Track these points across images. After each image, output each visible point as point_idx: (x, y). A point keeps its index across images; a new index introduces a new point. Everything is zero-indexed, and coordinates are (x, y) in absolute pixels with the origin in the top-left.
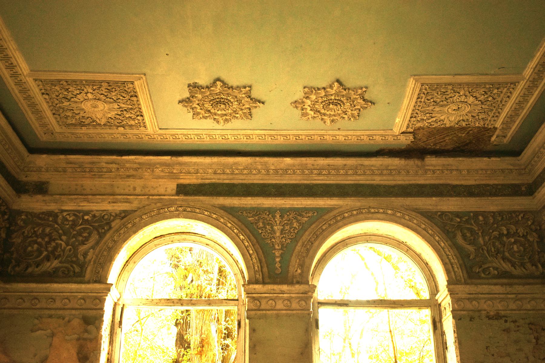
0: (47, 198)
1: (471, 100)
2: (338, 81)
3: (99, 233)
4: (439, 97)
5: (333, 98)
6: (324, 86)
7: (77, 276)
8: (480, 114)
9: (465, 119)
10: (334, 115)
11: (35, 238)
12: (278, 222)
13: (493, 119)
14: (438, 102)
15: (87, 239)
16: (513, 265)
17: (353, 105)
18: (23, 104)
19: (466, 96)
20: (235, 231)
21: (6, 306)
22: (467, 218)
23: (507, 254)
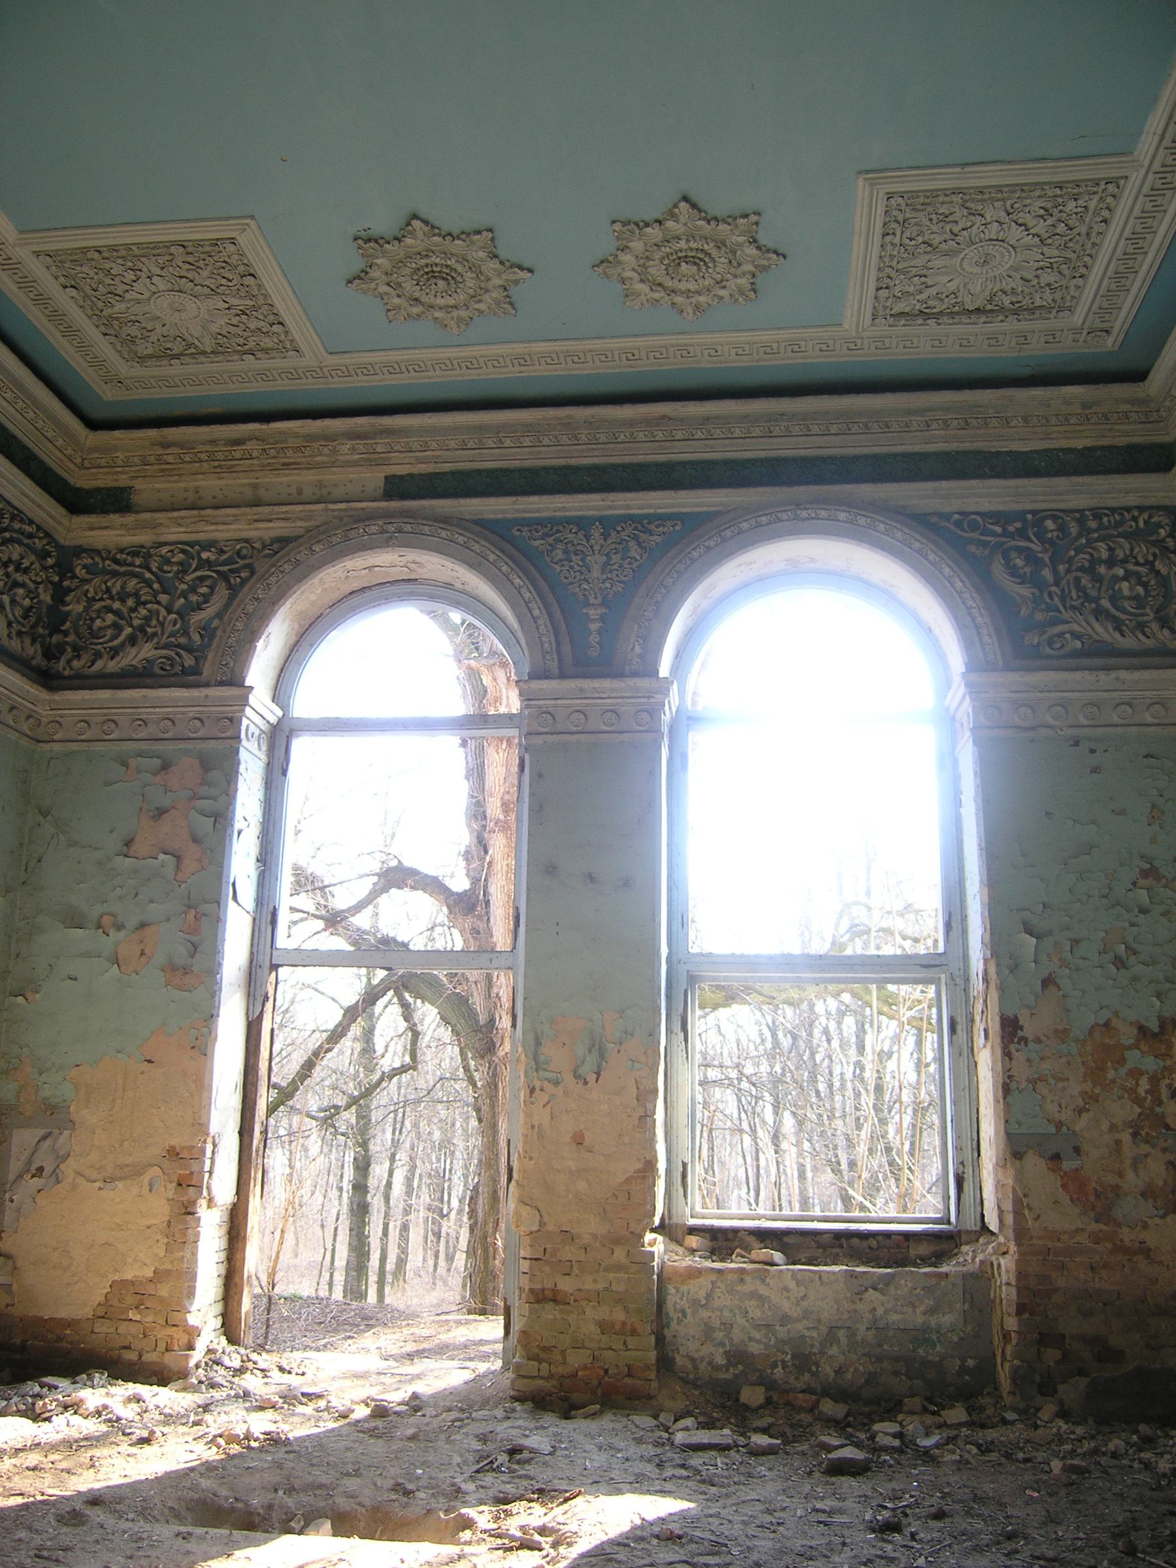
0: (130, 519)
1: (1015, 233)
2: (685, 199)
3: (230, 587)
4: (935, 228)
5: (683, 244)
6: (658, 216)
7: (188, 677)
8: (1040, 271)
9: (1008, 289)
10: (699, 293)
11: (108, 602)
12: (597, 548)
13: (1074, 282)
14: (935, 243)
15: (206, 598)
16: (1119, 627)
17: (735, 263)
18: (37, 317)
19: (1001, 223)
20: (504, 568)
21: (57, 737)
22: (1018, 525)
23: (1105, 603)
